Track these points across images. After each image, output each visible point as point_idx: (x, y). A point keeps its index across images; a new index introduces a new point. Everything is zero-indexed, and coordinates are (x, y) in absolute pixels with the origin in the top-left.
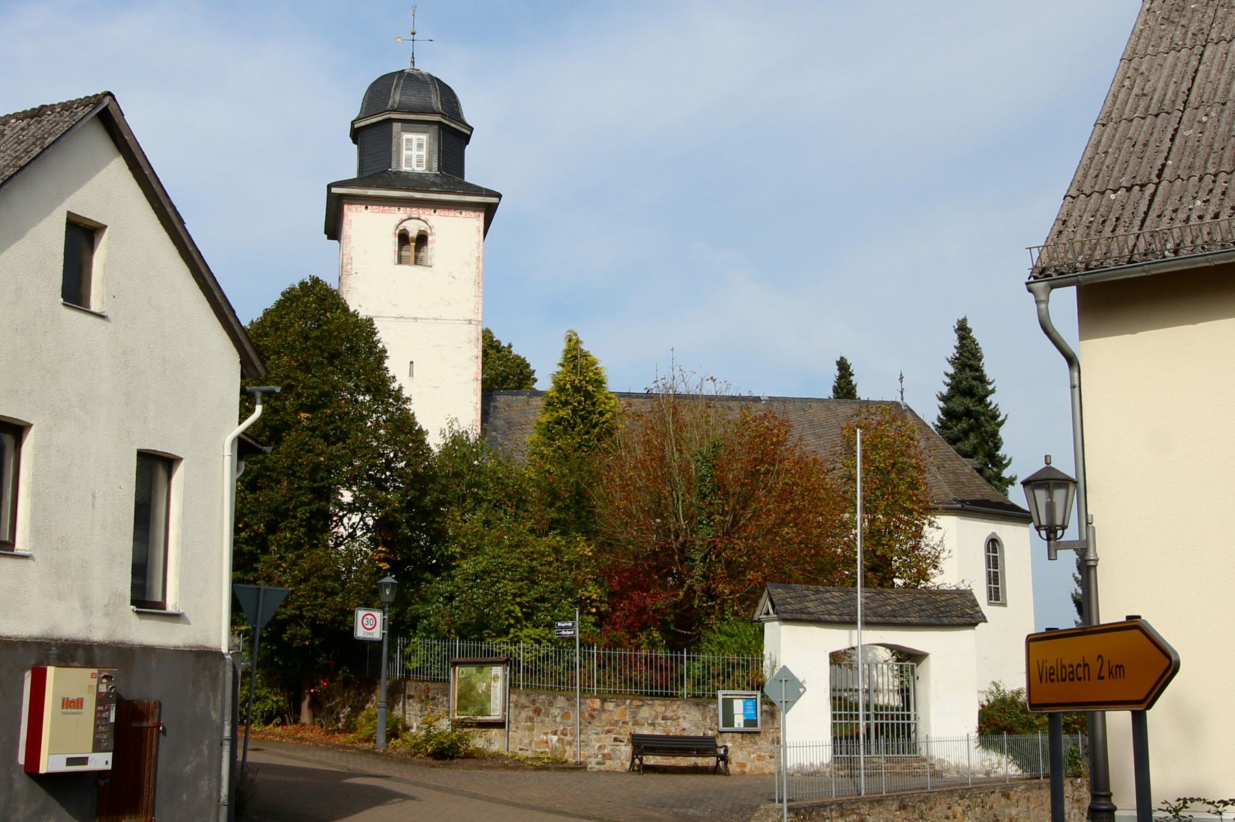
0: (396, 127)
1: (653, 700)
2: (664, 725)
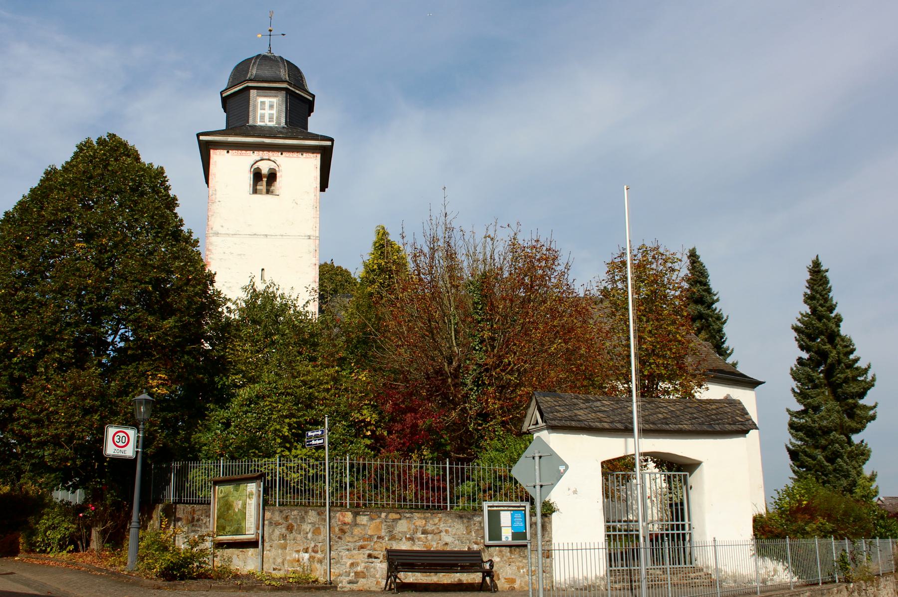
0: (253, 93)
1: (412, 513)
2: (425, 540)
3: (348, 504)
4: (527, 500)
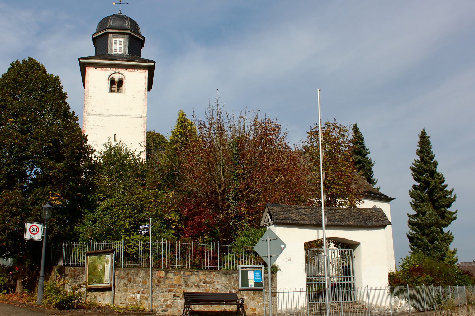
0: (110, 35)
1: (198, 271)
3: (162, 267)
4: (263, 264)
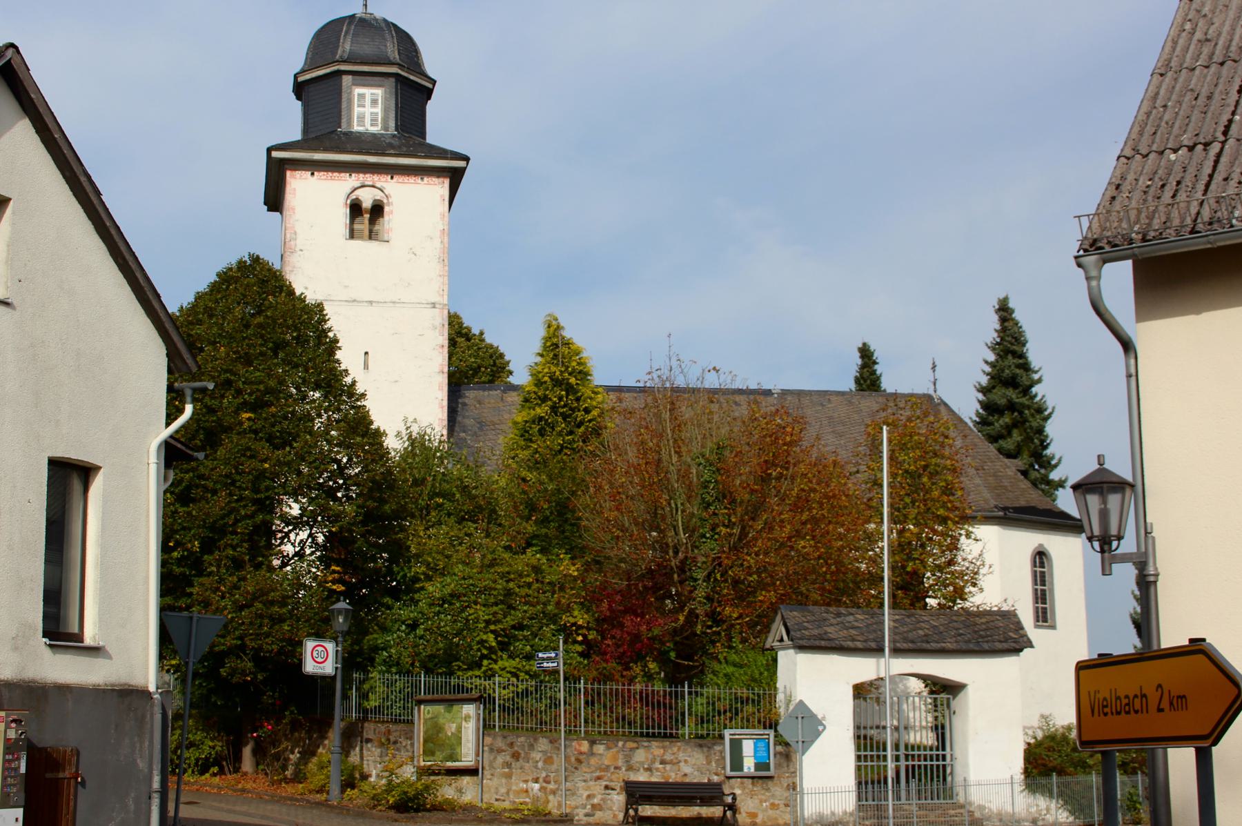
0: (347, 80)
1: (649, 741)
3: (583, 732)
4: (771, 728)
